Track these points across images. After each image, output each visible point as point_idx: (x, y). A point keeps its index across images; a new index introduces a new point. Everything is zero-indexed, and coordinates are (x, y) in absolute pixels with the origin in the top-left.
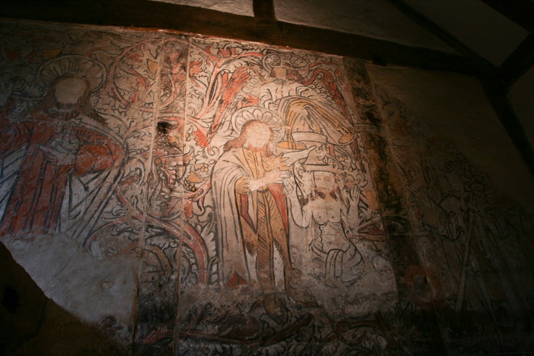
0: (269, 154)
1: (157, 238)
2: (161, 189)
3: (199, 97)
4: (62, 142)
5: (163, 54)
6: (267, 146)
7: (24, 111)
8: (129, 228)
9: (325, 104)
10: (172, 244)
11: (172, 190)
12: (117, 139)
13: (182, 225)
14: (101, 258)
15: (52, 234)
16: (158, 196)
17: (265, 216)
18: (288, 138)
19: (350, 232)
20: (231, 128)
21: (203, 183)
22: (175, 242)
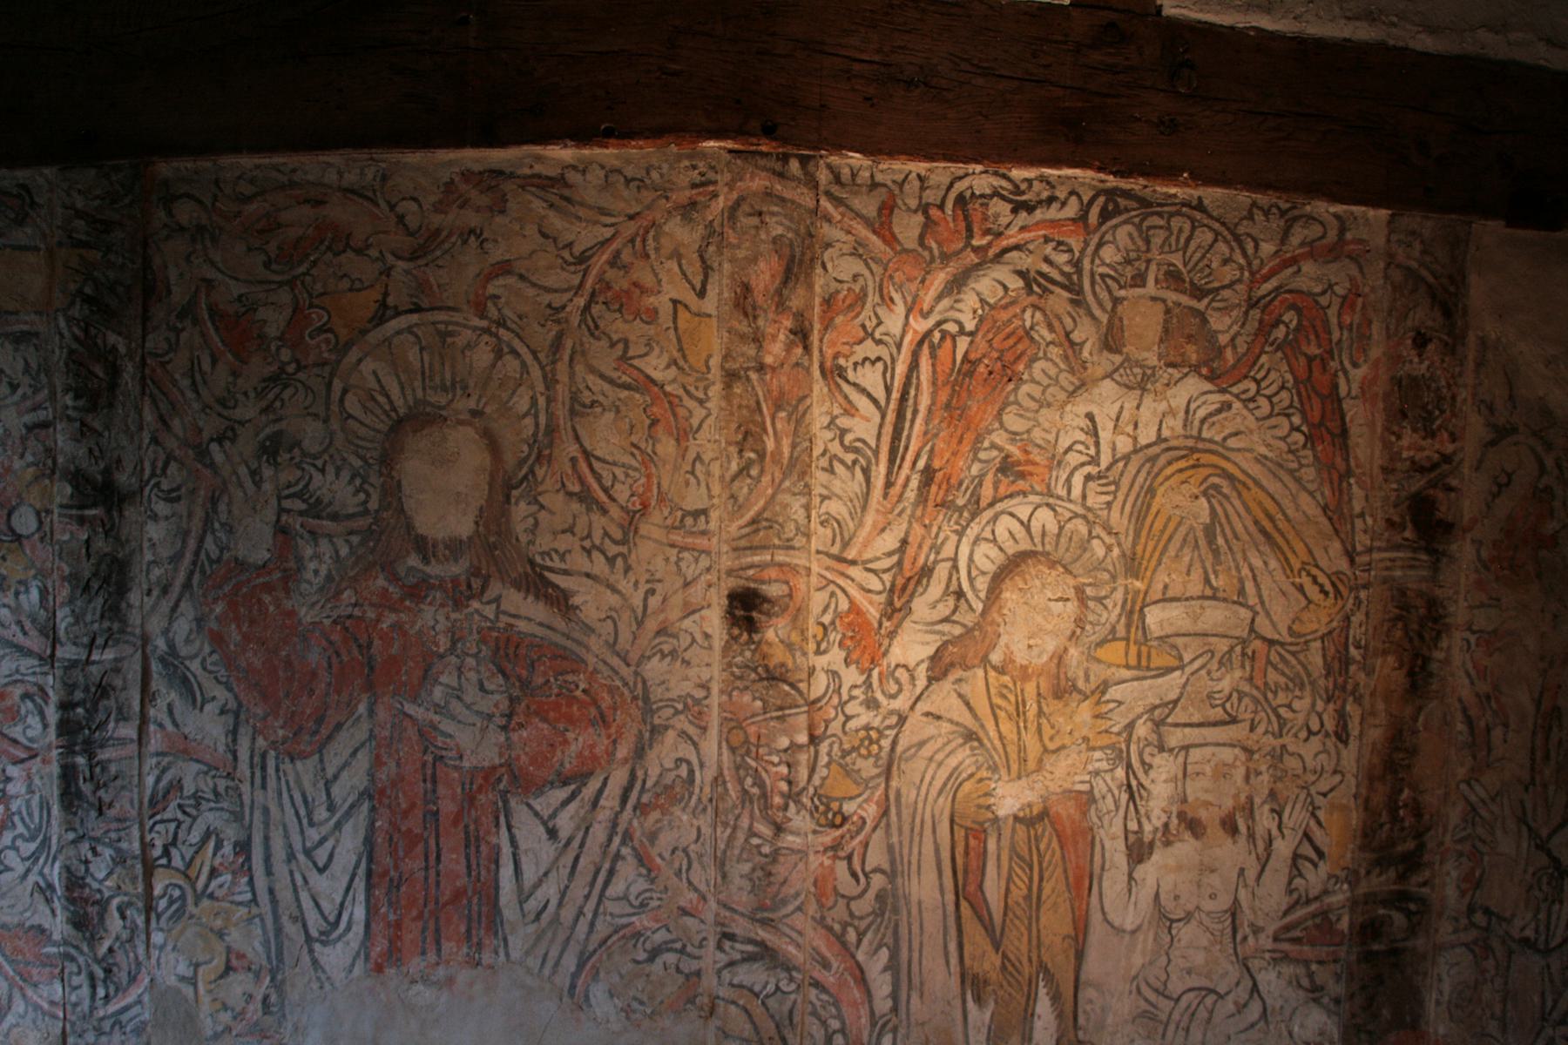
0: (1063, 689)
1: (745, 967)
2: (751, 826)
3: (855, 462)
4: (460, 689)
5: (726, 266)
6: (1060, 658)
7: (329, 578)
8: (673, 941)
9: (1275, 467)
10: (783, 985)
11: (779, 829)
12: (613, 669)
13: (810, 932)
14: (615, 1027)
15: (491, 967)
16: (743, 849)
17: (1028, 898)
18: (1128, 626)
19: (1251, 940)
20: (954, 587)
21: (865, 796)
22: (791, 979)
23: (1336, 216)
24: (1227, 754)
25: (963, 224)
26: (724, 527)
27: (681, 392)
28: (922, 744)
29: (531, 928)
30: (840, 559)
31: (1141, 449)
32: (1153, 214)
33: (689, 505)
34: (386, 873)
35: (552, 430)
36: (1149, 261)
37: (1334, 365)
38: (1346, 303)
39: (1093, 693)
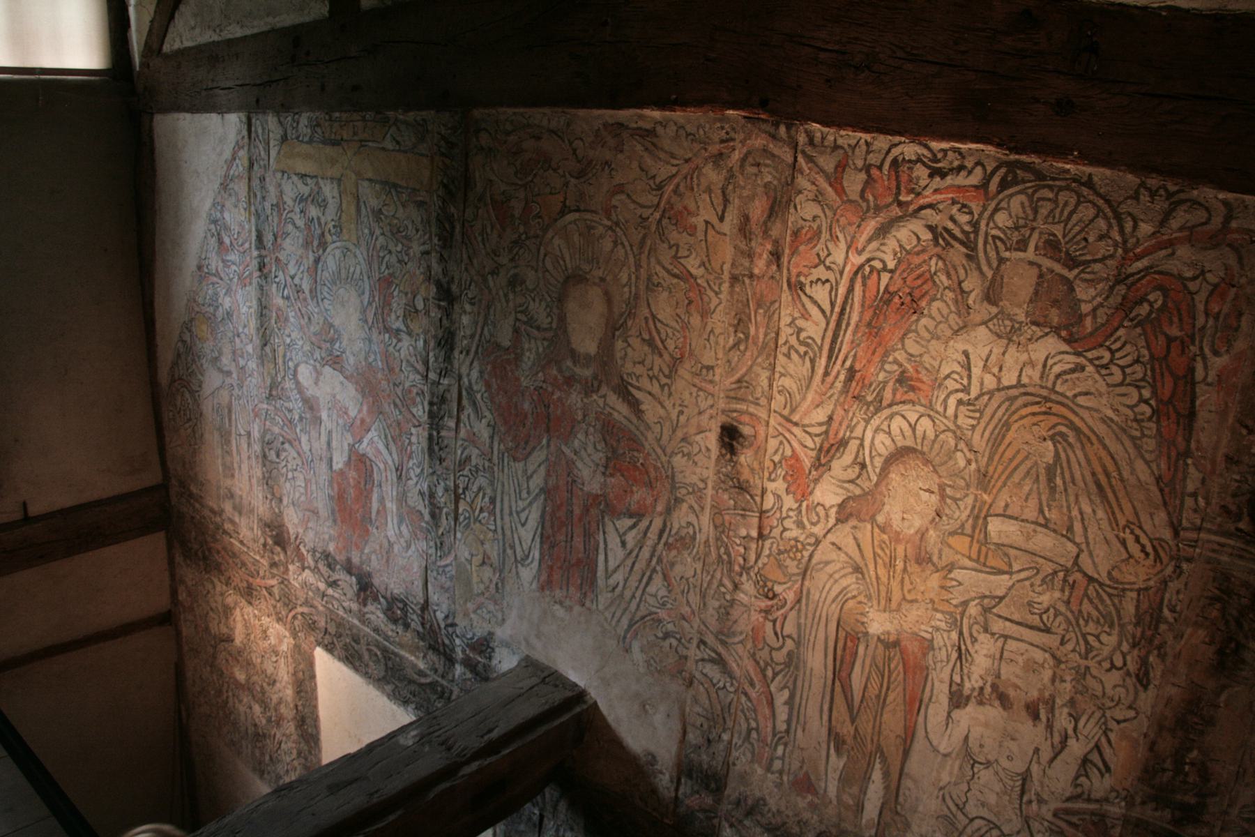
0: (923, 559)
3: (806, 353)
5: (736, 201)
6: (922, 534)
17: (878, 697)
18: (974, 528)
19: (1034, 806)
23: (1225, 203)
24: (1039, 656)
25: (894, 183)
26: (723, 381)
27: (705, 285)
28: (827, 563)
29: (609, 595)
30: (788, 420)
31: (1003, 389)
32: (1044, 187)
33: (706, 363)
34: (548, 537)
35: (637, 297)
36: (1033, 229)
37: (1194, 349)
38: (1216, 291)
39: (943, 568)
